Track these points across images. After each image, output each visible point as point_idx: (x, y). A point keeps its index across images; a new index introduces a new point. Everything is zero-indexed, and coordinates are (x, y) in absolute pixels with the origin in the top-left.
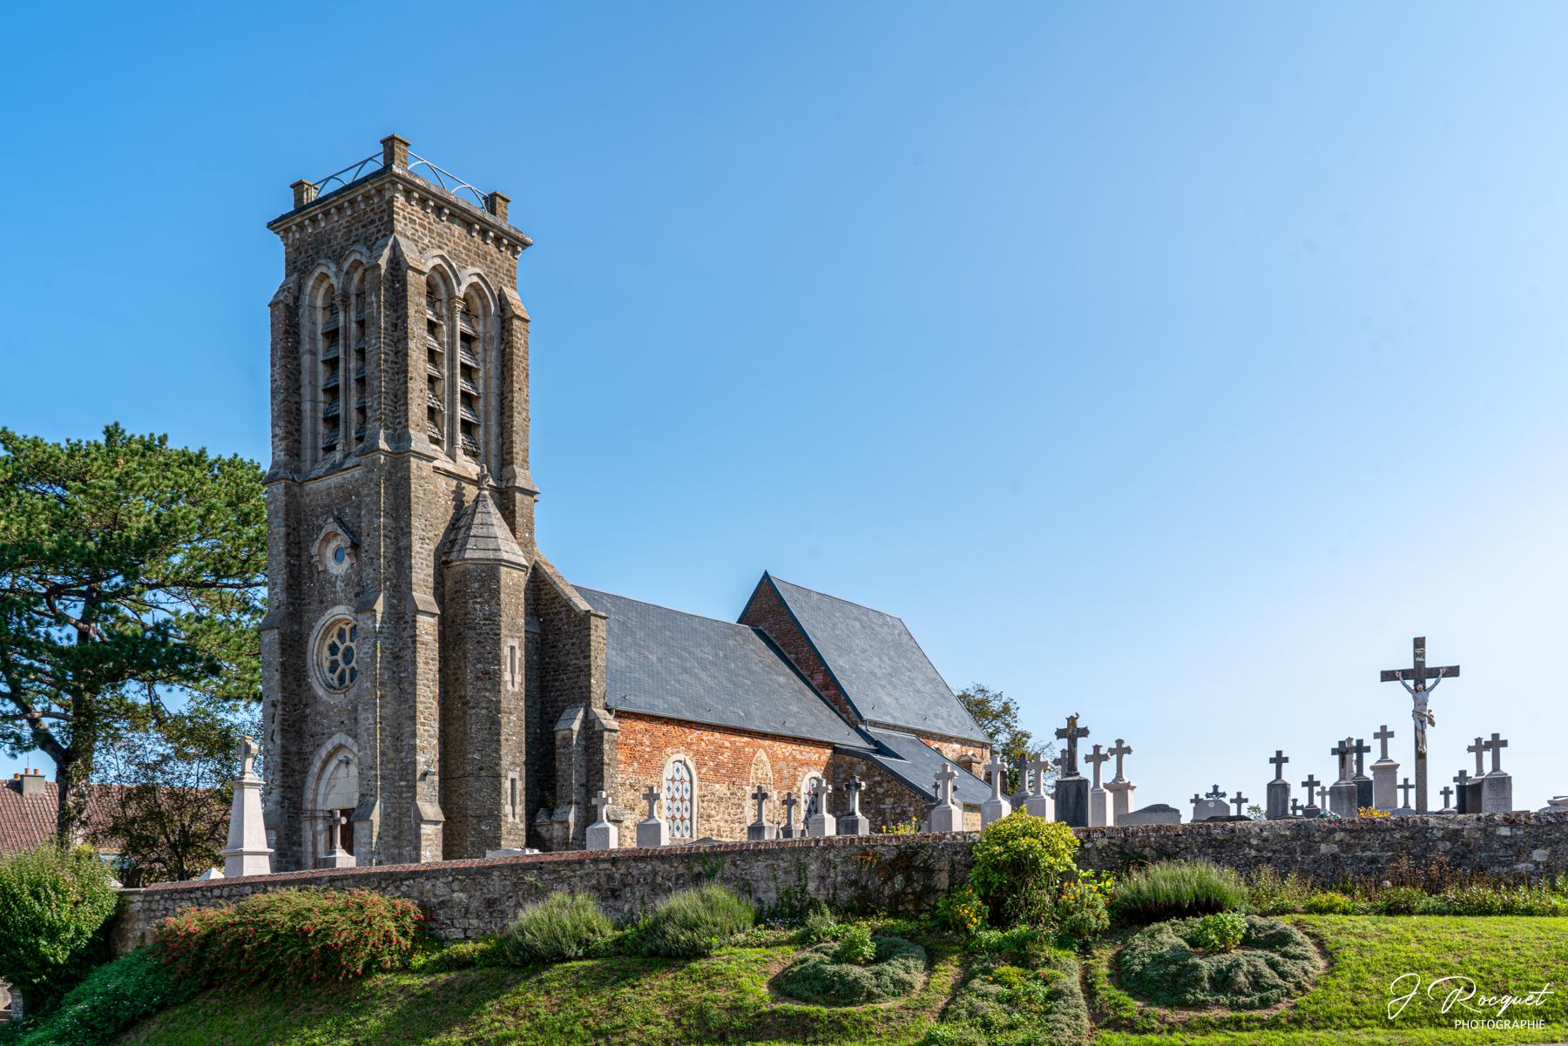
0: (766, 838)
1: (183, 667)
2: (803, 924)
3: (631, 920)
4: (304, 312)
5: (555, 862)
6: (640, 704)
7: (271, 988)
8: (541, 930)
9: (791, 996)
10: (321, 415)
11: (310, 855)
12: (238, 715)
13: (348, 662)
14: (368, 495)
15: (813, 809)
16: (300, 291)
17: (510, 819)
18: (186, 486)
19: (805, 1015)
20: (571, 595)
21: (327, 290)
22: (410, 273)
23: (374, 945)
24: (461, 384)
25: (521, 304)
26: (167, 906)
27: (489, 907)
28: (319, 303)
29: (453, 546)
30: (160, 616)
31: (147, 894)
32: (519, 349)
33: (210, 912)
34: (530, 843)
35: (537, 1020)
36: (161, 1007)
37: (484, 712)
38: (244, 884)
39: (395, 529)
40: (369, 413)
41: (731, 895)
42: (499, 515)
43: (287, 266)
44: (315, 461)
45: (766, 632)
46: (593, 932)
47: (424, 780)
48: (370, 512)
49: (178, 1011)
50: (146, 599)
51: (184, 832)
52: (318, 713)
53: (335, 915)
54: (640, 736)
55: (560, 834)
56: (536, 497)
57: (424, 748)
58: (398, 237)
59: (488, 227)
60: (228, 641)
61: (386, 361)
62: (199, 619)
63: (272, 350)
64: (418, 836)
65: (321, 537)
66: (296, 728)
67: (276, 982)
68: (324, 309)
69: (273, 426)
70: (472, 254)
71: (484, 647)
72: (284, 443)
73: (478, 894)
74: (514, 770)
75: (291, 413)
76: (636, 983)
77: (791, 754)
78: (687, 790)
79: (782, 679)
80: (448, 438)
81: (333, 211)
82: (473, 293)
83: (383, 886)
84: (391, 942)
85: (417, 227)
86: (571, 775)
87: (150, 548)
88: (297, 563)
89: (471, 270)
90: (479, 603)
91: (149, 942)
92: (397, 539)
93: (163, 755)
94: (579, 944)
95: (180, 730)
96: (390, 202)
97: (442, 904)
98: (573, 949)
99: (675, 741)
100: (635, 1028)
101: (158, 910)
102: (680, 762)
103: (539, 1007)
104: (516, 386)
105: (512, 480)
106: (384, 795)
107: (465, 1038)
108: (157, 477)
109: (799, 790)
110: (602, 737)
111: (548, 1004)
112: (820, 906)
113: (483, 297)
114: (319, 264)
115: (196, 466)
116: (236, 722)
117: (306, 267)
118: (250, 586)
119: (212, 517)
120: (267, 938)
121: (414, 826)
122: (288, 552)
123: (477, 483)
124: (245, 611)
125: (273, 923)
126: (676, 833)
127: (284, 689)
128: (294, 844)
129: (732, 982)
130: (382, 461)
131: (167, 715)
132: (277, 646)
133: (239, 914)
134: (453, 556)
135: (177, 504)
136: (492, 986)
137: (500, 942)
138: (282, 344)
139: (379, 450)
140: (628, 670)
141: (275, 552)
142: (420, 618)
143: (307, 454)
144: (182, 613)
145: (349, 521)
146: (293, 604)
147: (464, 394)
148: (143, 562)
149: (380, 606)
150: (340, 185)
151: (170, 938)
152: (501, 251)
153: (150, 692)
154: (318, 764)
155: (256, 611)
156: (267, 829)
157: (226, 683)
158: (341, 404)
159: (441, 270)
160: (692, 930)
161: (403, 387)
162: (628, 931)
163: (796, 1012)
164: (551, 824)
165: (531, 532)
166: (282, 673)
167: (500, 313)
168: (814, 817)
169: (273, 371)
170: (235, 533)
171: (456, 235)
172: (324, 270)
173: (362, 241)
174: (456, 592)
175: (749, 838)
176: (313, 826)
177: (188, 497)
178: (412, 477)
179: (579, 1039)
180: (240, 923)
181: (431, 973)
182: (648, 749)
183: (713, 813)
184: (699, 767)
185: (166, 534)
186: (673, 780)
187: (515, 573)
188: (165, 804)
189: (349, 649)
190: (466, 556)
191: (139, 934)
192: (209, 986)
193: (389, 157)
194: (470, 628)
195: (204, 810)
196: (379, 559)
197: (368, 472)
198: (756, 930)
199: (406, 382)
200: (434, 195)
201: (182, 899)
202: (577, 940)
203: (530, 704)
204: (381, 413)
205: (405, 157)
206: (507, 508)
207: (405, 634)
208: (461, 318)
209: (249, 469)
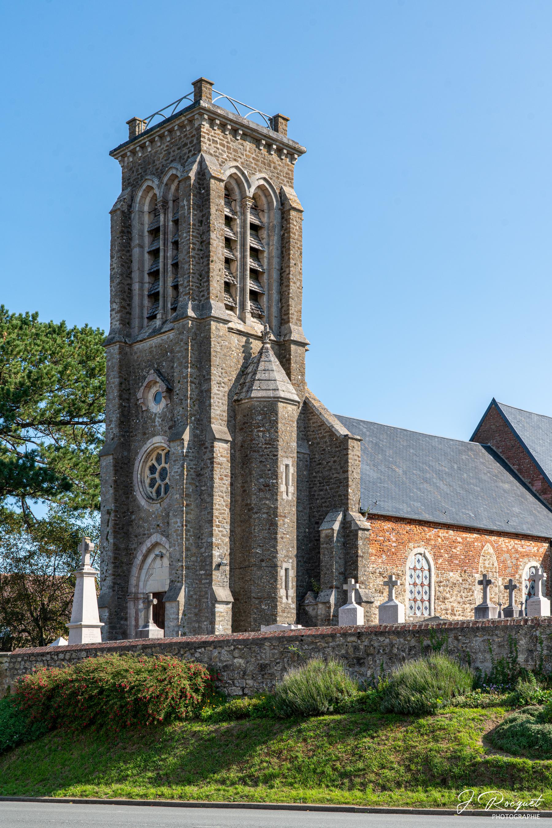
0: (490, 617)
1: (45, 485)
2: (513, 690)
3: (372, 683)
4: (135, 216)
5: (313, 636)
6: (388, 509)
7: (98, 730)
8: (300, 689)
9: (501, 749)
10: (146, 293)
11: (133, 628)
12: (84, 520)
13: (163, 479)
14: (179, 352)
15: (531, 594)
16: (132, 200)
17: (284, 600)
18: (50, 350)
19: (513, 766)
20: (333, 423)
21: (152, 198)
22: (212, 181)
23: (173, 699)
24: (250, 263)
25: (296, 198)
26: (26, 666)
27: (262, 671)
28: (146, 208)
29: (242, 388)
30: (31, 447)
31: (12, 657)
32: (294, 234)
33: (56, 671)
34: (298, 622)
35: (296, 762)
36: (19, 743)
37: (264, 516)
38: (81, 650)
39: (199, 376)
40: (181, 289)
41: (454, 664)
42: (278, 363)
43: (123, 182)
44: (141, 327)
45: (494, 448)
46: (342, 692)
47: (219, 570)
48: (180, 364)
49: (31, 747)
50: (22, 435)
51: (43, 609)
52: (141, 518)
53: (145, 675)
54: (388, 533)
55: (323, 612)
56: (307, 347)
57: (219, 544)
58: (204, 155)
59: (237, 126)
60: (77, 465)
61: (193, 249)
62: (58, 449)
63: (112, 246)
64: (213, 614)
65: (145, 384)
66: (125, 530)
67: (101, 726)
68: (150, 213)
69: (112, 302)
70: (259, 163)
71: (265, 466)
72: (119, 315)
73: (253, 660)
74: (287, 562)
75: (125, 292)
76: (375, 735)
77: (514, 547)
78: (426, 577)
79: (507, 486)
80: (240, 305)
81: (157, 138)
82: (260, 193)
83: (182, 653)
84: (186, 697)
85: (218, 146)
86: (332, 565)
87: (23, 397)
88: (127, 405)
89: (259, 175)
90: (261, 431)
91: (13, 693)
92: (200, 384)
93: (29, 551)
94: (330, 701)
95: (44, 533)
96: (199, 129)
97: (226, 668)
98: (325, 706)
99: (416, 538)
100: (373, 772)
101: (19, 669)
102: (421, 554)
103: (297, 751)
104: (292, 262)
105: (288, 335)
106: (188, 581)
107: (240, 775)
108: (30, 344)
109: (521, 577)
110: (357, 535)
111: (305, 749)
112: (528, 675)
113: (267, 195)
114: (146, 179)
115: (58, 334)
116: (83, 526)
117: (137, 182)
118: (95, 423)
119: (68, 372)
120: (95, 692)
121: (210, 605)
122: (121, 397)
123: (261, 338)
124: (91, 442)
125: (100, 680)
126: (417, 611)
127: (116, 500)
128: (122, 619)
129: (453, 736)
130: (190, 325)
131: (35, 521)
132: (112, 468)
133: (76, 673)
134: (243, 395)
135: (44, 363)
136: (262, 733)
137: (269, 698)
138: (119, 241)
139: (187, 317)
140: (379, 481)
141: (111, 397)
142: (216, 444)
143: (136, 323)
144: (45, 445)
145: (165, 372)
146: (123, 436)
147: (252, 271)
148: (18, 408)
149: (186, 436)
150: (161, 119)
151: (27, 691)
152: (282, 159)
153: (23, 504)
154: (140, 558)
155: (99, 441)
156: (100, 607)
157: (76, 496)
158: (161, 283)
159: (236, 177)
160: (420, 692)
161: (206, 268)
162: (369, 692)
163: (505, 763)
164: (317, 604)
165: (303, 375)
166: (115, 488)
167: (280, 207)
168: (532, 600)
169: (112, 261)
170: (84, 384)
171: (248, 149)
172: (149, 183)
173: (178, 159)
174: (244, 424)
175: (476, 616)
176: (136, 605)
177: (52, 358)
178: (212, 336)
179: (328, 778)
180: (77, 680)
181: (216, 722)
182: (394, 544)
183: (448, 595)
184: (436, 559)
185: (35, 386)
186: (415, 569)
187: (290, 408)
188: (30, 587)
189: (164, 469)
190: (252, 395)
191: (6, 687)
192: (53, 728)
193: (198, 94)
194: (255, 451)
195: (58, 593)
196: (186, 400)
197: (179, 334)
198: (474, 693)
199: (208, 264)
200: (231, 121)
201: (37, 661)
202: (329, 698)
203: (300, 509)
204: (190, 289)
205: (210, 94)
206: (285, 357)
207: (205, 457)
208: (251, 213)
209: (96, 335)
